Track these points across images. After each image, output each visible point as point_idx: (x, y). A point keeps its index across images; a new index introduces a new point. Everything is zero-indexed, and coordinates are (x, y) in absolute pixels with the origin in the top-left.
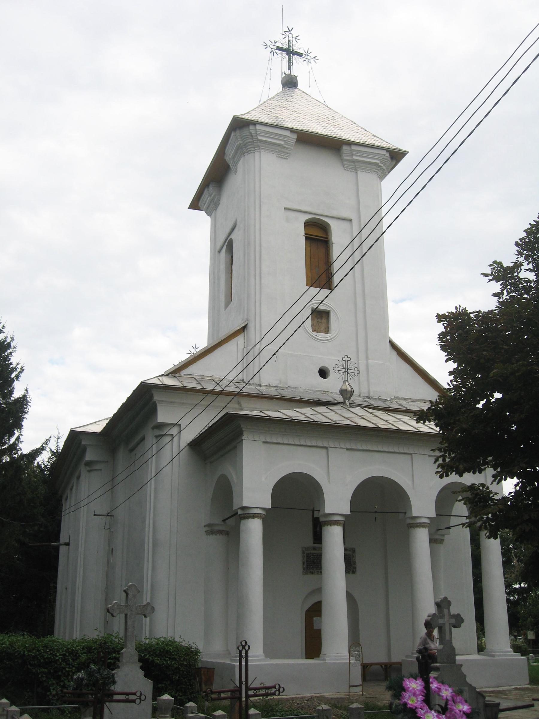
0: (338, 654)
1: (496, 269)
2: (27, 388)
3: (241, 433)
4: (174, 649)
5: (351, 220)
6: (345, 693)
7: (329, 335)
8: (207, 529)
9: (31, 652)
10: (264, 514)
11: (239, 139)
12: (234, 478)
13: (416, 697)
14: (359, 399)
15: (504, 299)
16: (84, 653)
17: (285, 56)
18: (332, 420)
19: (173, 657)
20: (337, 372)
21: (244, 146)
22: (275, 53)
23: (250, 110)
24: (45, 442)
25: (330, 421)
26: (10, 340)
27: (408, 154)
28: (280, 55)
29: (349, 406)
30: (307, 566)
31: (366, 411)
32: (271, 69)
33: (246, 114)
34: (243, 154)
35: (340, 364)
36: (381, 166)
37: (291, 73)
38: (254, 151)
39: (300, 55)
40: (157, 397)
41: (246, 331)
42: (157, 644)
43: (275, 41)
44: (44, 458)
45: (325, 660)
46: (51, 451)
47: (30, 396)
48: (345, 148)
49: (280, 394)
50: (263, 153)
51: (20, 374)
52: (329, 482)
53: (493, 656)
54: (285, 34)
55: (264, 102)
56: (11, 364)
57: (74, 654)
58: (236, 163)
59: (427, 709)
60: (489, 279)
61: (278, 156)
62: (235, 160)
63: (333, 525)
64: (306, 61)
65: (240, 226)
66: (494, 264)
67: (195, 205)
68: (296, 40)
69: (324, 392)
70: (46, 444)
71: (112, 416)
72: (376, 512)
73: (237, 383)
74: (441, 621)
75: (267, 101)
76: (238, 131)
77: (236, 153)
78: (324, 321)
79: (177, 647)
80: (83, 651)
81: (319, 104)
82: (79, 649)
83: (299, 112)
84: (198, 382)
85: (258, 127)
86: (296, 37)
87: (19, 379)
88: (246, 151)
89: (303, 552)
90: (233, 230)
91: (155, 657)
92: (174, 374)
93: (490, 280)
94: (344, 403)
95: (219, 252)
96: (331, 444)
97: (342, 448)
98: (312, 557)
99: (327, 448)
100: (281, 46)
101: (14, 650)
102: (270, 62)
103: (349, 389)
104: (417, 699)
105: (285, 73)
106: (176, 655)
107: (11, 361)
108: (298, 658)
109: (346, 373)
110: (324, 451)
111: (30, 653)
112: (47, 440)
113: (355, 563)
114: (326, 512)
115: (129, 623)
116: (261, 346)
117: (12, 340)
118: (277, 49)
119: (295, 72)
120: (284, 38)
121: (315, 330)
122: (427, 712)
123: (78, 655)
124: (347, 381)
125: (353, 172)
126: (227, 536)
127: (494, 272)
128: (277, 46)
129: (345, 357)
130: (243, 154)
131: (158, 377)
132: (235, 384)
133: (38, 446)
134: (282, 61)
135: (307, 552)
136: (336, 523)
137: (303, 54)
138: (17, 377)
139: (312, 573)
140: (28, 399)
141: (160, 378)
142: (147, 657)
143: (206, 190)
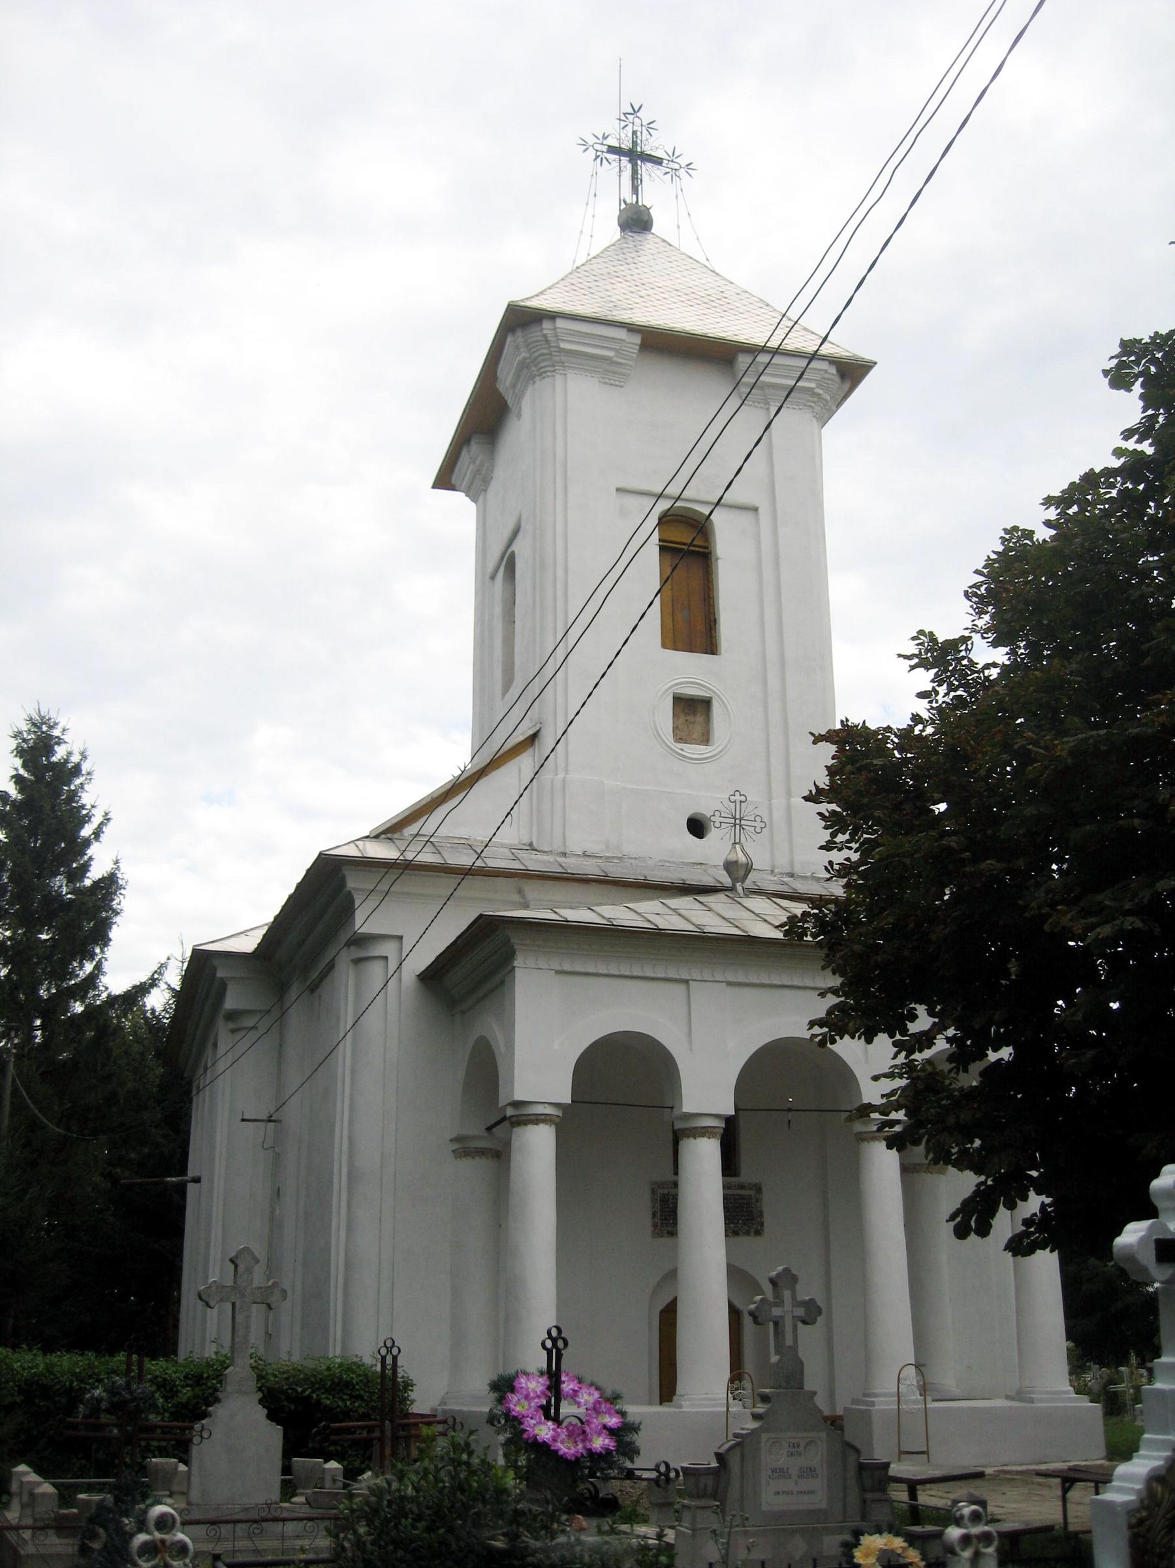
0: (707, 1396)
1: (926, 644)
2: (118, 858)
3: (510, 956)
4: (361, 1378)
5: (755, 509)
7: (709, 748)
8: (455, 1146)
9: (86, 1384)
10: (558, 1116)
11: (522, 350)
12: (500, 1047)
13: (528, 1401)
14: (772, 878)
15: (940, 702)
16: (188, 1385)
17: (625, 165)
18: (697, 926)
19: (357, 1393)
20: (758, 819)
21: (533, 362)
22: (604, 160)
23: (546, 287)
24: (159, 968)
25: (692, 928)
26: (80, 757)
27: (877, 366)
28: (615, 164)
29: (741, 895)
30: (661, 1220)
31: (775, 903)
32: (595, 195)
33: (537, 295)
34: (532, 378)
36: (818, 395)
37: (637, 202)
38: (554, 374)
39: (658, 161)
40: (353, 882)
41: (536, 743)
42: (329, 1369)
43: (604, 134)
44: (157, 1001)
45: (680, 1406)
46: (170, 988)
47: (124, 876)
48: (743, 360)
49: (603, 871)
50: (571, 375)
51: (101, 829)
52: (691, 1050)
53: (1031, 1401)
54: (625, 119)
55: (578, 268)
56: (83, 807)
57: (168, 1388)
58: (519, 398)
59: (540, 1418)
60: (910, 666)
61: (603, 381)
62: (517, 391)
63: (699, 1136)
64: (670, 175)
65: (527, 527)
66: (920, 636)
67: (444, 480)
68: (649, 130)
69: (699, 866)
70: (160, 974)
71: (272, 919)
72: (789, 1110)
73: (519, 851)
74: (776, 1312)
75: (583, 265)
76: (519, 333)
77: (517, 377)
78: (700, 719)
79: (366, 1375)
80: (185, 1381)
81: (696, 265)
82: (178, 1378)
83: (650, 285)
84: (437, 850)
85: (560, 323)
86: (649, 124)
87: (101, 839)
88: (536, 373)
89: (653, 1192)
90: (516, 533)
91: (323, 1394)
92: (389, 835)
93: (913, 668)
94: (732, 889)
95: (493, 578)
96: (696, 975)
97: (706, 981)
99: (686, 982)
100: (618, 145)
101: (54, 1379)
102: (594, 178)
103: (742, 859)
104: (529, 1404)
105: (624, 201)
106: (364, 1390)
107: (83, 801)
108: (642, 1404)
109: (738, 827)
110: (682, 988)
111: (82, 1385)
112: (162, 964)
113: (761, 1214)
114: (685, 1110)
115: (240, 1318)
116: (567, 774)
117: (84, 756)
118: (608, 152)
119: (647, 198)
120: (623, 128)
121: (680, 739)
122: (539, 1423)
123: (175, 1389)
124: (739, 843)
125: (762, 408)
126: (495, 1159)
127: (923, 651)
128: (609, 146)
129: (734, 795)
130: (532, 379)
131: (357, 842)
132: (513, 854)
133: (143, 977)
134: (620, 176)
135: (661, 1191)
136: (705, 1132)
137: (662, 159)
138: (97, 834)
140: (120, 882)
141: (360, 843)
142: (307, 1393)
143: (464, 452)
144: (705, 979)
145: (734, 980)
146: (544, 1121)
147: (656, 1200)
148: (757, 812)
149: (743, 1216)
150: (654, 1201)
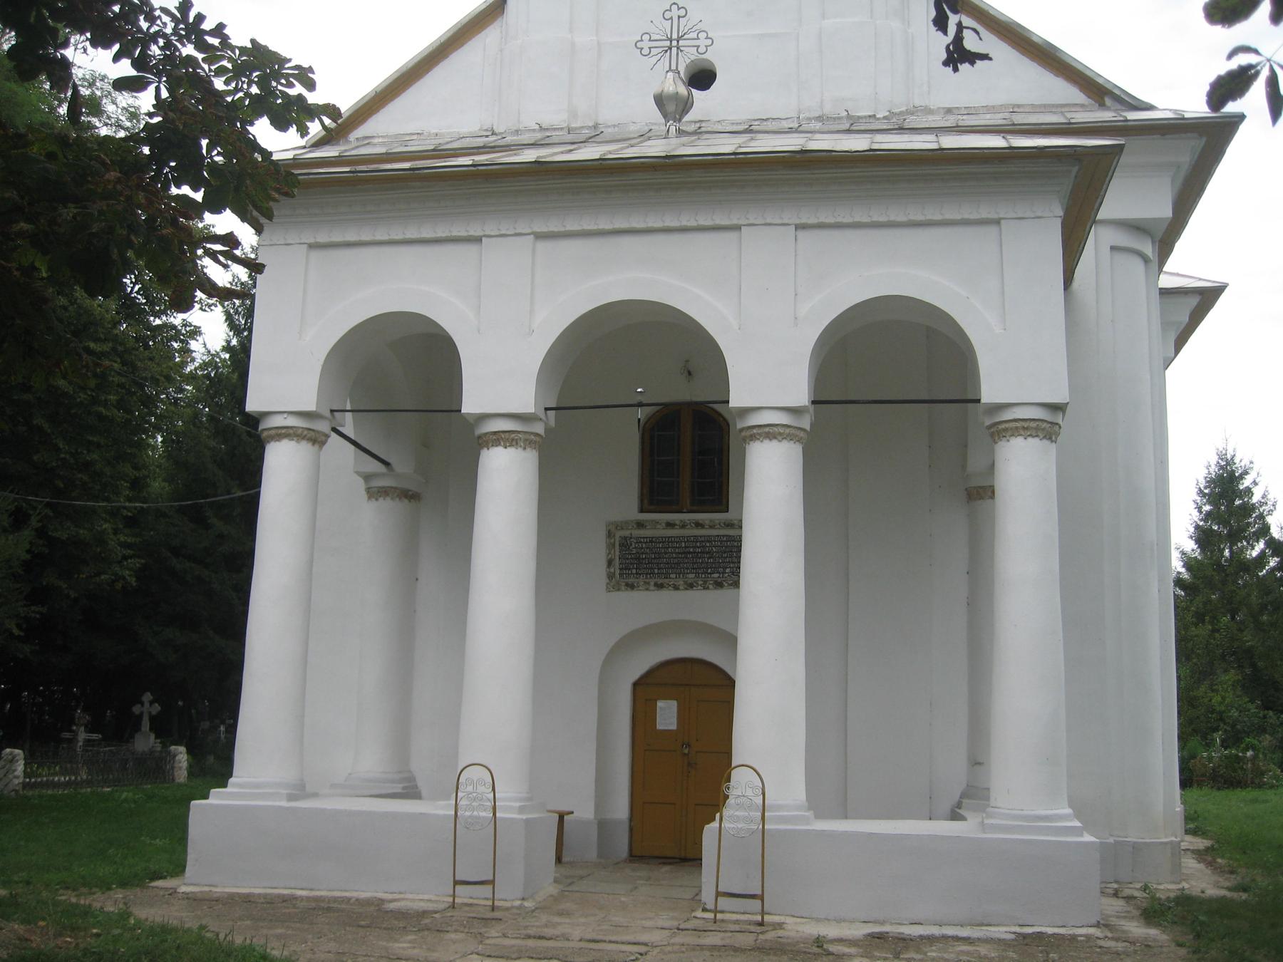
6: (471, 898)
30: (620, 569)
35: (658, 31)
89: (610, 534)
96: (491, 228)
98: (635, 548)
109: (674, 50)
139: (631, 587)
144: (503, 232)
145: (545, 229)
146: (287, 436)
147: (614, 545)
148: (700, 26)
149: (733, 563)
150: (611, 546)
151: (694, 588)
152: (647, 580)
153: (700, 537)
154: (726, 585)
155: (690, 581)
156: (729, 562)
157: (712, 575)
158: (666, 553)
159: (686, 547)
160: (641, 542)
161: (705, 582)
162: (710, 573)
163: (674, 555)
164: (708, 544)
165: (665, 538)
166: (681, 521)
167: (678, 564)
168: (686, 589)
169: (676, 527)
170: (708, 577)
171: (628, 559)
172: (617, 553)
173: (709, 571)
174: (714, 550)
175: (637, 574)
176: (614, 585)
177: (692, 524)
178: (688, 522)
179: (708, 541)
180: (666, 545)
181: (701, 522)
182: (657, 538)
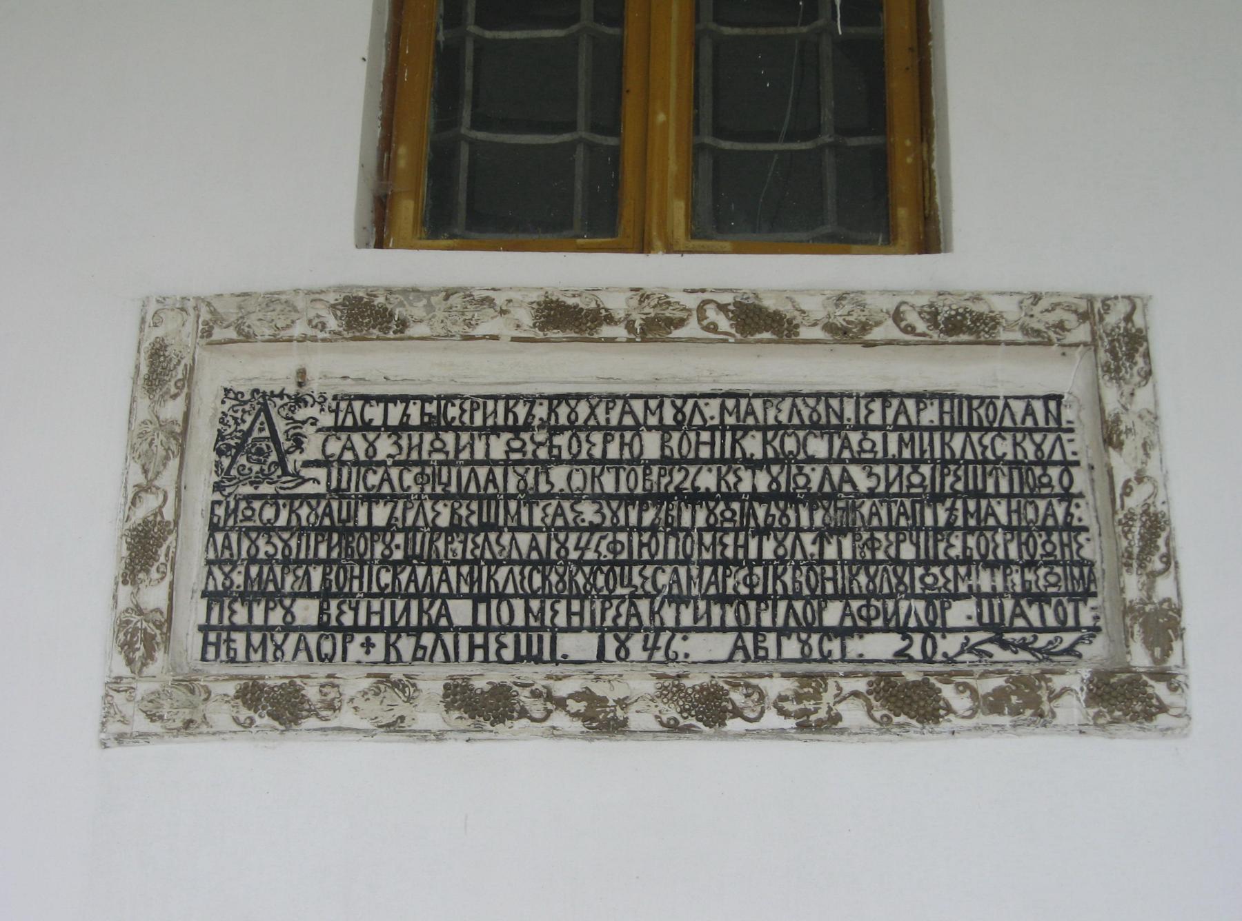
30: (212, 597)
147: (181, 435)
151: (734, 725)
152: (397, 672)
153: (767, 397)
154: (961, 703)
155: (697, 679)
156: (967, 560)
157: (855, 646)
158: (531, 498)
159: (665, 461)
160: (365, 427)
161: (812, 683)
162: (842, 633)
163: (589, 512)
164: (818, 447)
165: (531, 400)
166: (643, 296)
167: (615, 566)
168: (673, 728)
169: (606, 331)
170: (825, 658)
171: (268, 529)
172: (201, 493)
173: (832, 615)
174: (864, 484)
175: (322, 627)
176: (154, 699)
177: (712, 314)
178: (692, 302)
179: (827, 430)
180: (534, 444)
181: (770, 303)
182: (479, 401)
